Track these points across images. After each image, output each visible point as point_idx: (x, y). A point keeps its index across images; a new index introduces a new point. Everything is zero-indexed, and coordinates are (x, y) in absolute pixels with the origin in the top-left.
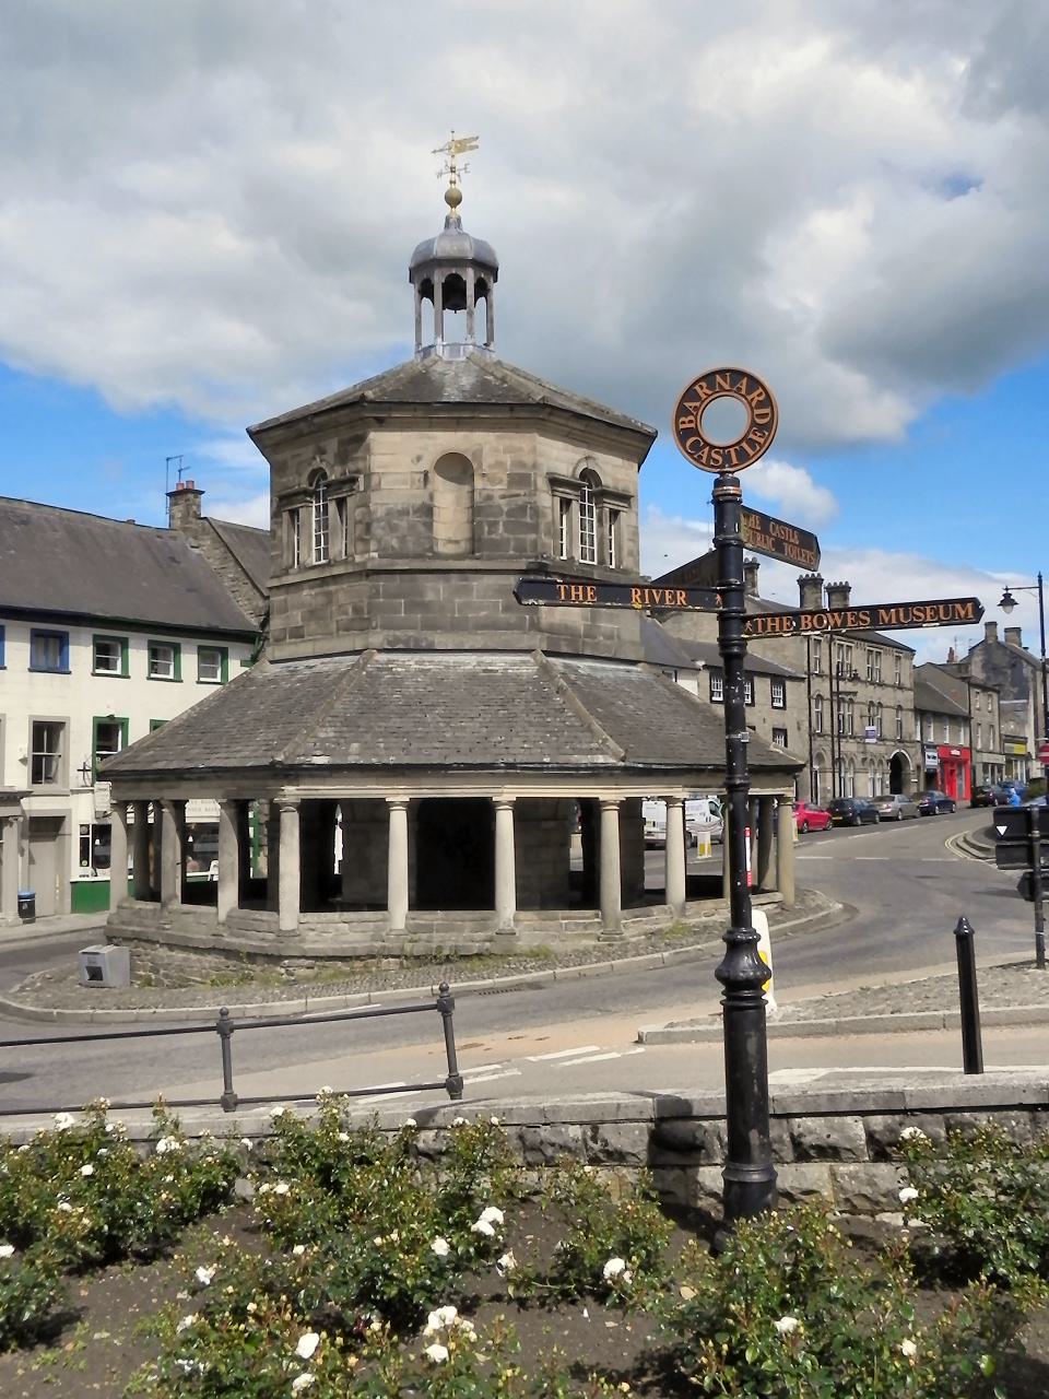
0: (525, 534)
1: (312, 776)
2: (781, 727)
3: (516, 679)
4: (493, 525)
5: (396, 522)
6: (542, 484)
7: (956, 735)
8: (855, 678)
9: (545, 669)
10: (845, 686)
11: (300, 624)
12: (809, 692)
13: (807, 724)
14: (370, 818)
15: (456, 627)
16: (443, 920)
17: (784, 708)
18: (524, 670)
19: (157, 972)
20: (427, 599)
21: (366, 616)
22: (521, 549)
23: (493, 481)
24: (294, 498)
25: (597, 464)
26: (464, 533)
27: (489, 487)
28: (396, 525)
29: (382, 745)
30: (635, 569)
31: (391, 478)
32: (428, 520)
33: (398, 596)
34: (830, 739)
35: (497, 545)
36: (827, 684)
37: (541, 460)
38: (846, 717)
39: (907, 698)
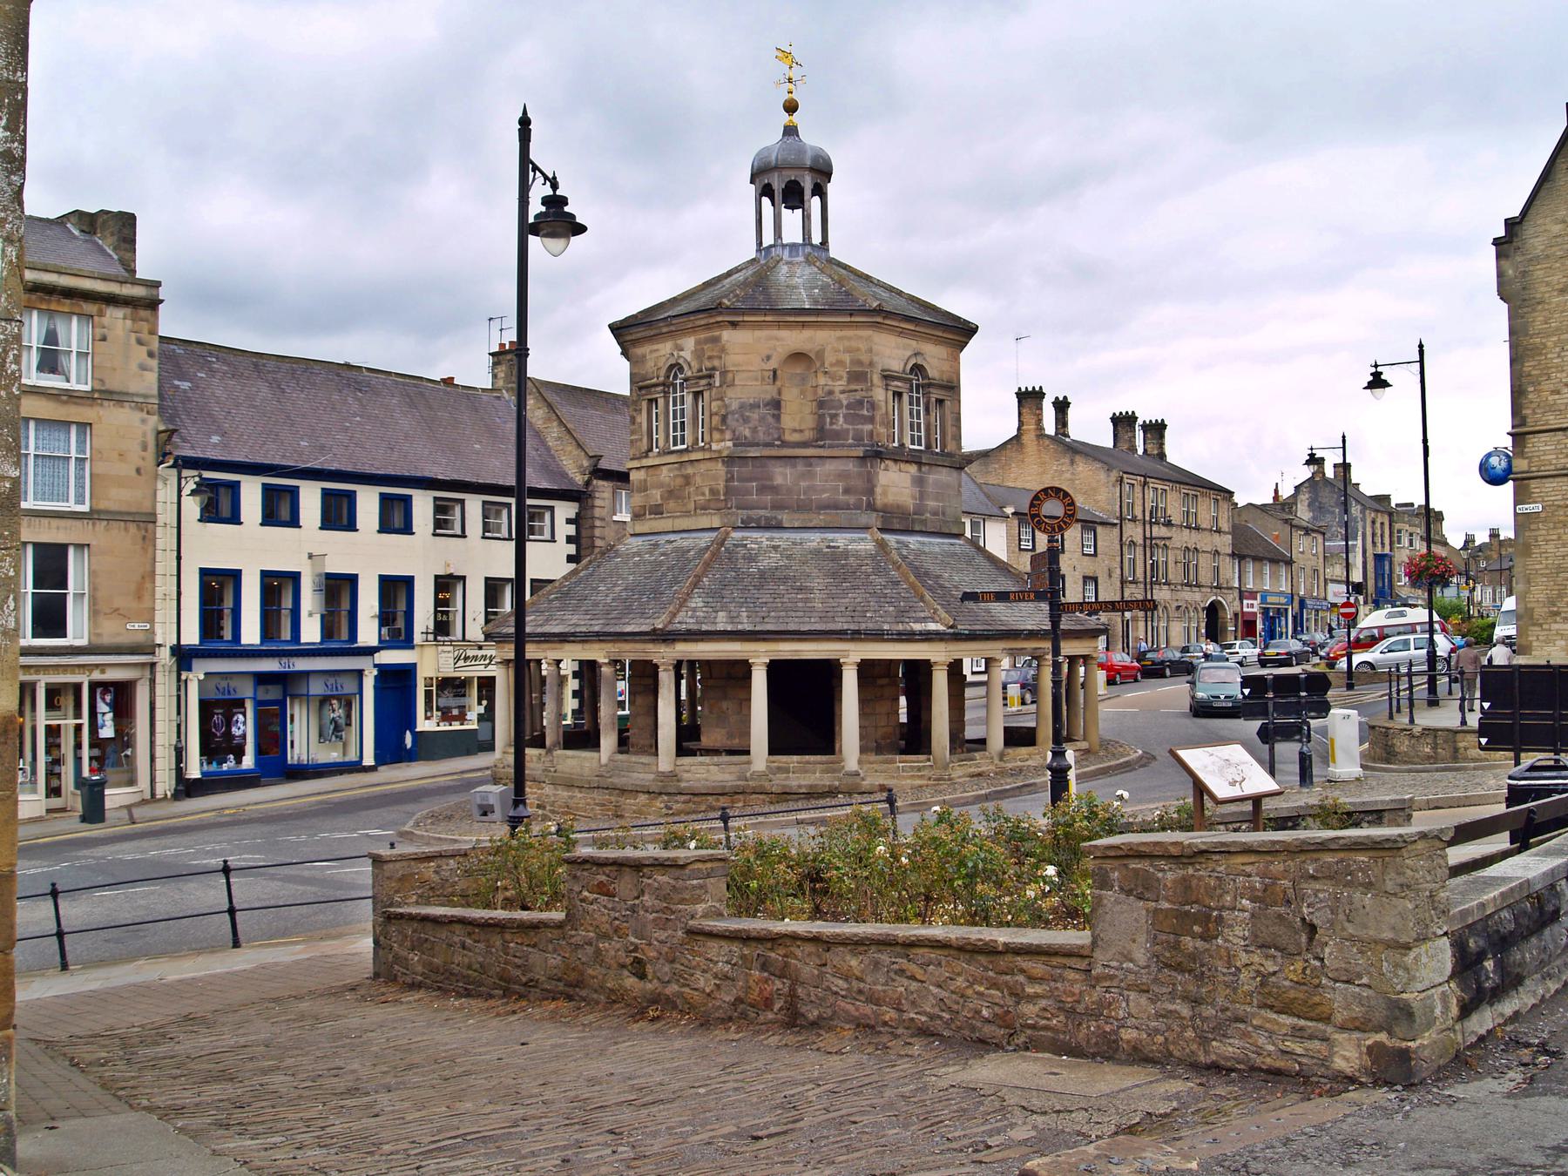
0: (862, 424)
1: (685, 640)
2: (1091, 575)
3: (856, 554)
4: (834, 417)
5: (747, 414)
6: (876, 379)
7: (1275, 577)
8: (1169, 524)
9: (882, 545)
10: (1158, 531)
11: (659, 502)
12: (1121, 540)
13: (1118, 571)
14: (738, 672)
15: (802, 507)
16: (798, 763)
17: (1095, 555)
18: (861, 546)
19: (544, 808)
20: (775, 483)
21: (722, 498)
22: (858, 438)
23: (833, 378)
24: (653, 389)
25: (924, 359)
26: (809, 422)
27: (830, 383)
28: (748, 417)
29: (745, 614)
30: (957, 452)
31: (745, 375)
32: (776, 412)
33: (751, 480)
34: (1142, 586)
35: (837, 435)
36: (1140, 530)
37: (876, 359)
38: (1160, 563)
39: (1225, 543)
